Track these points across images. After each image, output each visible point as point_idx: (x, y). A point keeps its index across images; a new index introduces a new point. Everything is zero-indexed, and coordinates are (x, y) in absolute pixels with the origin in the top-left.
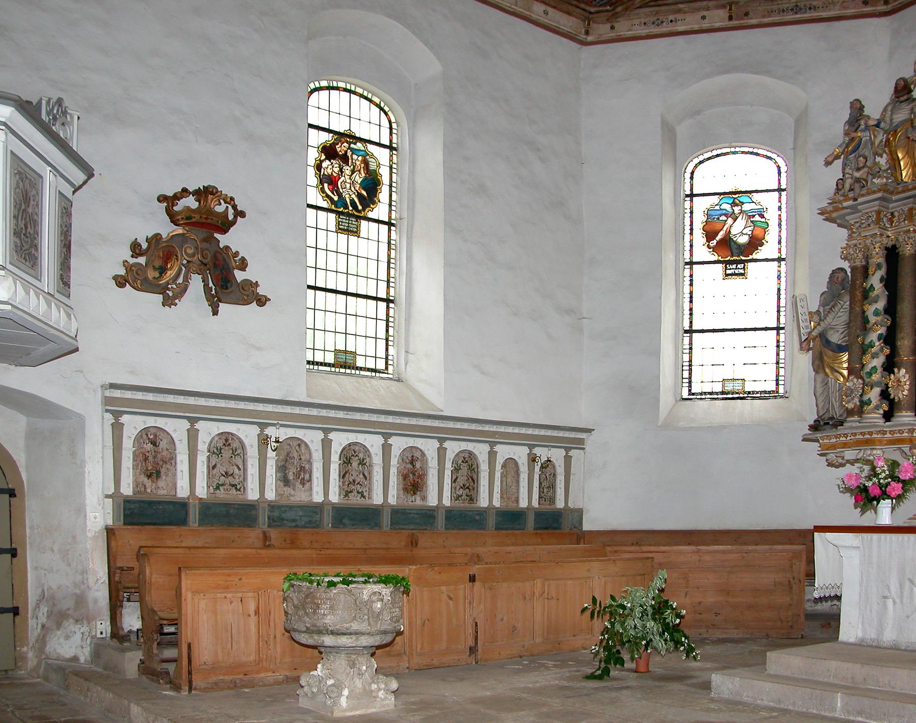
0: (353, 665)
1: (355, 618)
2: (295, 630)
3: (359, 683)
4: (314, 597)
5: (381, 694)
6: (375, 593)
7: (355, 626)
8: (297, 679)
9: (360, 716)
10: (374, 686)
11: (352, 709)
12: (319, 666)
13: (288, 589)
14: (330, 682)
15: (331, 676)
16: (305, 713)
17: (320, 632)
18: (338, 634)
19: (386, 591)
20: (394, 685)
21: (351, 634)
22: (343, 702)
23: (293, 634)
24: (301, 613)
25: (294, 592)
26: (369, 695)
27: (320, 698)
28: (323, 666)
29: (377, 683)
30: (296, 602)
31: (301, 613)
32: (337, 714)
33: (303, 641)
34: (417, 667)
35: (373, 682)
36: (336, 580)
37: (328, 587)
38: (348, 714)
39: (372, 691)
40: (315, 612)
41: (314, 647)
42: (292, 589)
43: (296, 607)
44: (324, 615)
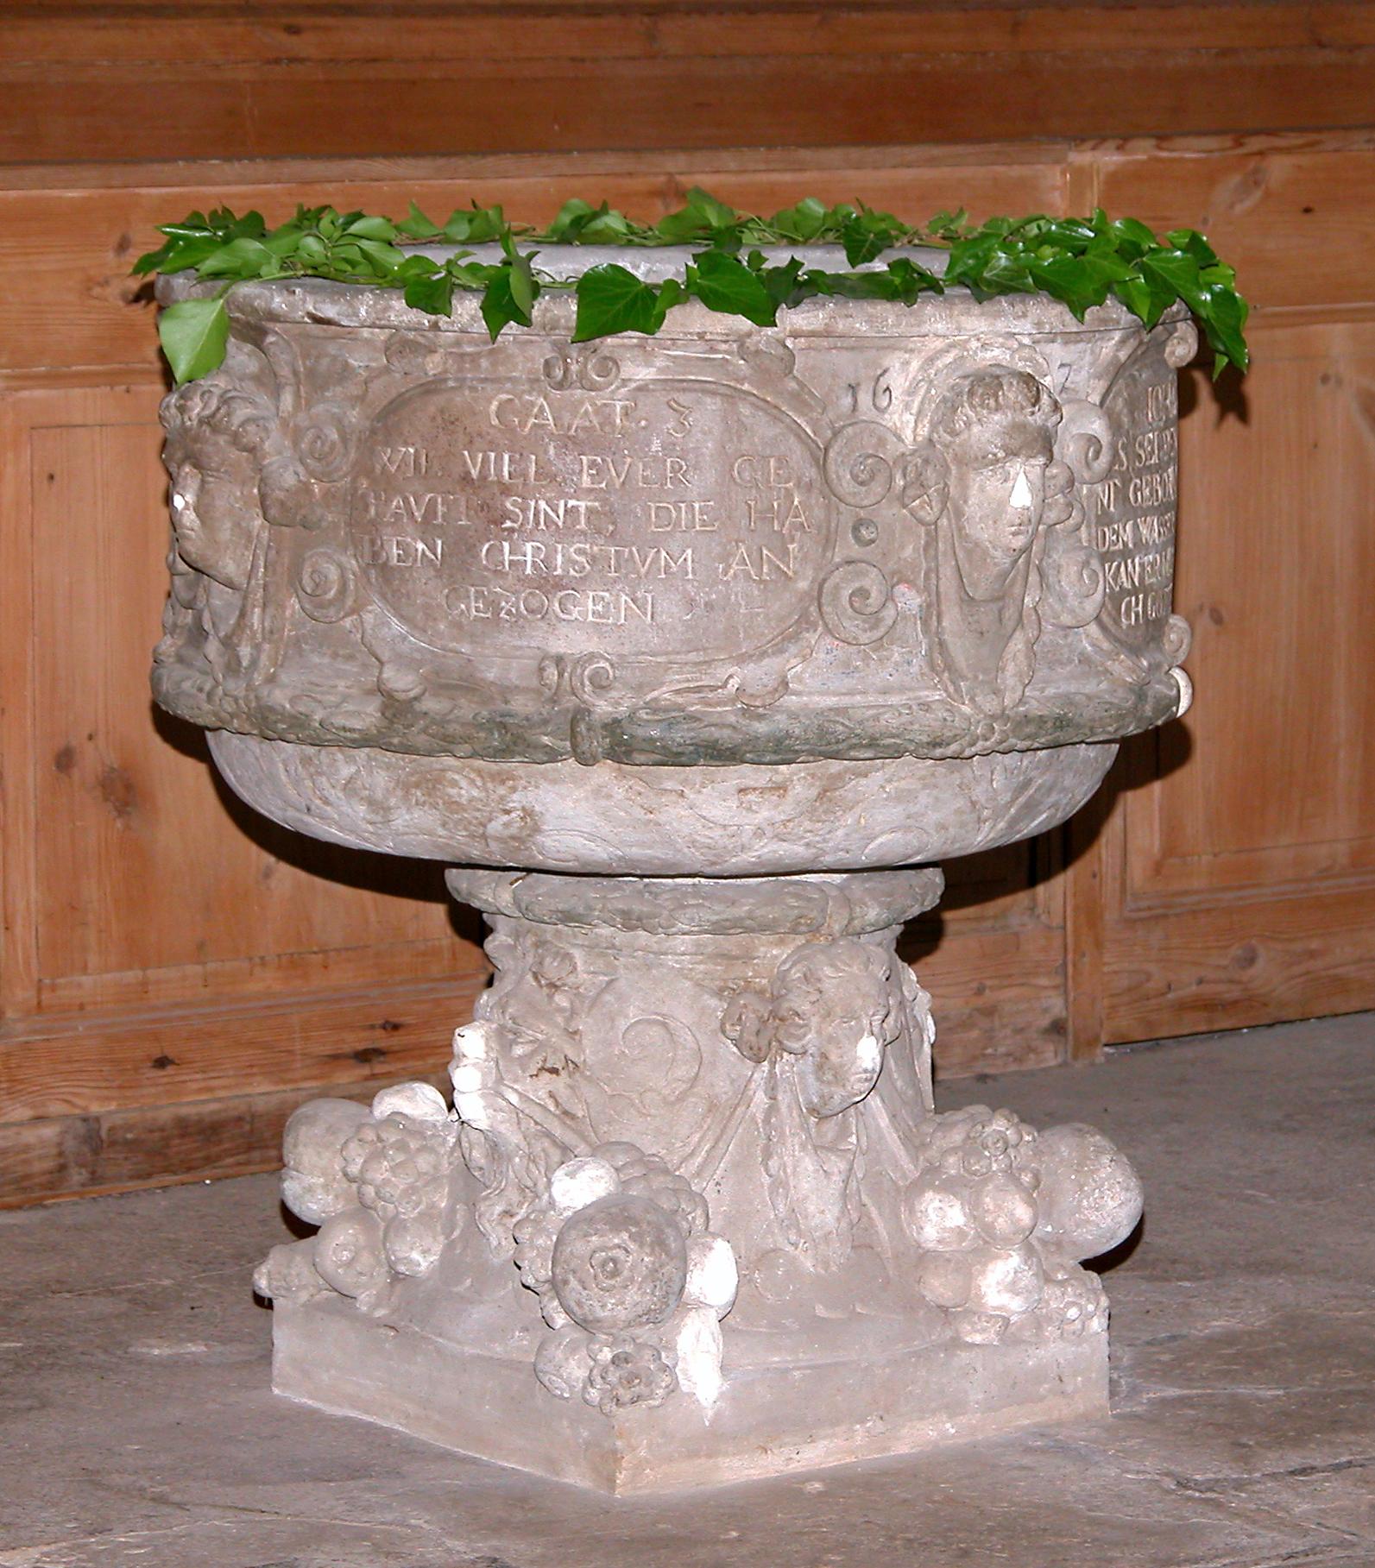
0: (765, 1028)
1: (811, 613)
2: (268, 725)
3: (814, 1188)
4: (455, 427)
5: (1001, 1284)
6: (986, 384)
7: (816, 682)
8: (260, 1142)
9: (844, 1486)
10: (940, 1218)
11: (770, 1428)
12: (472, 1042)
13: (213, 358)
14: (580, 1187)
15: (570, 1135)
16: (355, 1472)
17: (508, 740)
18: (675, 758)
19: (1068, 356)
20: (1108, 1204)
21: (781, 751)
22: (699, 1362)
23: (238, 756)
24: (334, 566)
25: (269, 380)
26: (888, 1284)
27: (479, 1328)
28: (504, 1038)
29: (965, 1187)
30: (288, 478)
31: (334, 566)
32: (651, 1476)
33: (345, 822)
34: (1126, 1023)
35: (931, 1177)
36: (654, 267)
37: (593, 327)
38: (741, 1469)
39: (924, 1258)
40: (459, 564)
41: (415, 878)
42: (242, 357)
43: (288, 517)
44: (547, 583)
